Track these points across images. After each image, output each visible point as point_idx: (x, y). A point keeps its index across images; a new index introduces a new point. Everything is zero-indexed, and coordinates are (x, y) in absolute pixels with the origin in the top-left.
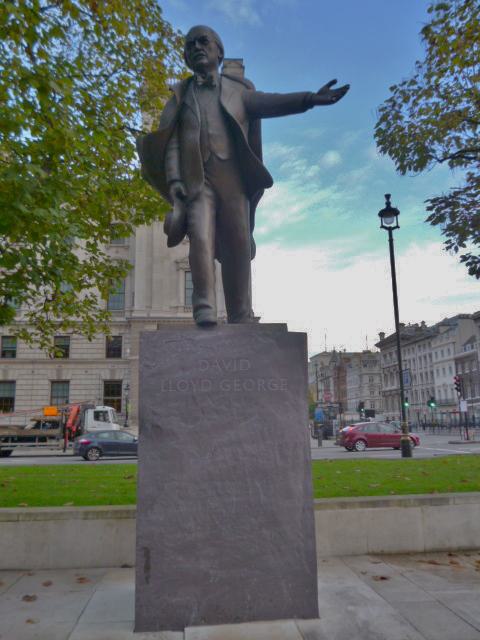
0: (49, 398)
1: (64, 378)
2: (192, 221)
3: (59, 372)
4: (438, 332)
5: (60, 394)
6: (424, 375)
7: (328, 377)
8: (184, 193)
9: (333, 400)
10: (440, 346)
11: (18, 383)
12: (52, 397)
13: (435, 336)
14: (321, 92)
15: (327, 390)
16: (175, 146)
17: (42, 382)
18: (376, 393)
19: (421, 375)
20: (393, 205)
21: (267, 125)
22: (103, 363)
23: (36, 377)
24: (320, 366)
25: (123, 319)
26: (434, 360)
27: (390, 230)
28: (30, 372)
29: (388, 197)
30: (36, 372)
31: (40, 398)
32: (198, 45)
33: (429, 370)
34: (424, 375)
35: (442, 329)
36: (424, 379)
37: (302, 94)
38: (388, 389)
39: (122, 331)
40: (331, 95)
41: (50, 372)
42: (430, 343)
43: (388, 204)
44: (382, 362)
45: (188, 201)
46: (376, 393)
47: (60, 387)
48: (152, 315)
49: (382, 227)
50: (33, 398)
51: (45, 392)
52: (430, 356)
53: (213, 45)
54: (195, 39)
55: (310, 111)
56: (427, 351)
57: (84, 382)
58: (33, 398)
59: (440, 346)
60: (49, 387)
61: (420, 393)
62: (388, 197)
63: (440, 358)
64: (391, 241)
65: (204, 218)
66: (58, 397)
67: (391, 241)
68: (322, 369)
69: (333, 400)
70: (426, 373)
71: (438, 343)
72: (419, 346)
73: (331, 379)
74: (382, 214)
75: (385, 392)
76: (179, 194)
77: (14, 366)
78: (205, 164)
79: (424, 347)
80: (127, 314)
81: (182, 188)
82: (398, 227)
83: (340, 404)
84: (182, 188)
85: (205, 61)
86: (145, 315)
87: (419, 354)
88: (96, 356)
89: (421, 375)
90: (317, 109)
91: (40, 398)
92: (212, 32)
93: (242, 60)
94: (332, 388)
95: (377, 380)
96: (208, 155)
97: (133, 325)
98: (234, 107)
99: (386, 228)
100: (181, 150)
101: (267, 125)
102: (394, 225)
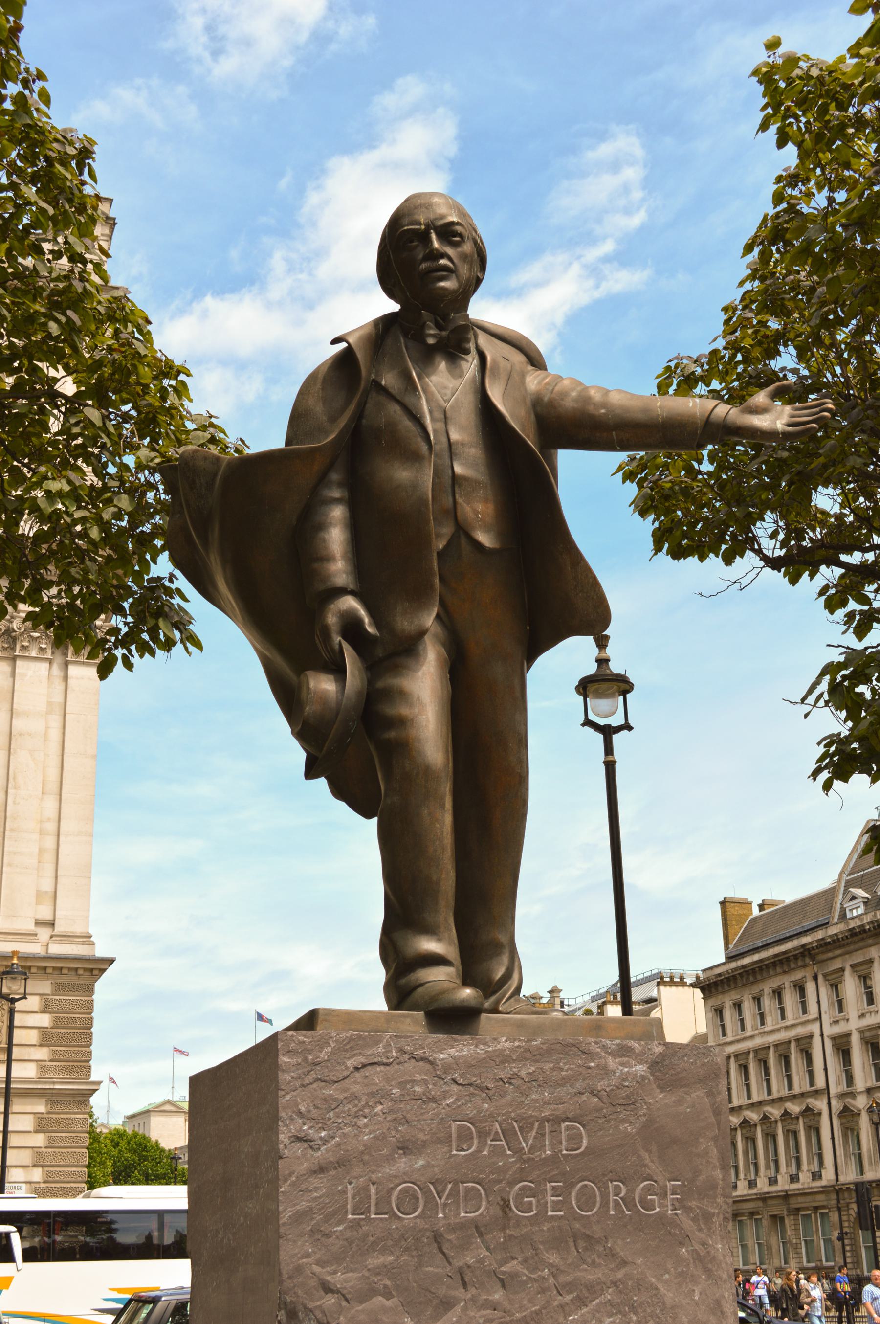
20: (615, 667)
27: (608, 732)
49: (588, 723)
64: (610, 767)
67: (610, 767)
82: (627, 727)
102: (617, 720)
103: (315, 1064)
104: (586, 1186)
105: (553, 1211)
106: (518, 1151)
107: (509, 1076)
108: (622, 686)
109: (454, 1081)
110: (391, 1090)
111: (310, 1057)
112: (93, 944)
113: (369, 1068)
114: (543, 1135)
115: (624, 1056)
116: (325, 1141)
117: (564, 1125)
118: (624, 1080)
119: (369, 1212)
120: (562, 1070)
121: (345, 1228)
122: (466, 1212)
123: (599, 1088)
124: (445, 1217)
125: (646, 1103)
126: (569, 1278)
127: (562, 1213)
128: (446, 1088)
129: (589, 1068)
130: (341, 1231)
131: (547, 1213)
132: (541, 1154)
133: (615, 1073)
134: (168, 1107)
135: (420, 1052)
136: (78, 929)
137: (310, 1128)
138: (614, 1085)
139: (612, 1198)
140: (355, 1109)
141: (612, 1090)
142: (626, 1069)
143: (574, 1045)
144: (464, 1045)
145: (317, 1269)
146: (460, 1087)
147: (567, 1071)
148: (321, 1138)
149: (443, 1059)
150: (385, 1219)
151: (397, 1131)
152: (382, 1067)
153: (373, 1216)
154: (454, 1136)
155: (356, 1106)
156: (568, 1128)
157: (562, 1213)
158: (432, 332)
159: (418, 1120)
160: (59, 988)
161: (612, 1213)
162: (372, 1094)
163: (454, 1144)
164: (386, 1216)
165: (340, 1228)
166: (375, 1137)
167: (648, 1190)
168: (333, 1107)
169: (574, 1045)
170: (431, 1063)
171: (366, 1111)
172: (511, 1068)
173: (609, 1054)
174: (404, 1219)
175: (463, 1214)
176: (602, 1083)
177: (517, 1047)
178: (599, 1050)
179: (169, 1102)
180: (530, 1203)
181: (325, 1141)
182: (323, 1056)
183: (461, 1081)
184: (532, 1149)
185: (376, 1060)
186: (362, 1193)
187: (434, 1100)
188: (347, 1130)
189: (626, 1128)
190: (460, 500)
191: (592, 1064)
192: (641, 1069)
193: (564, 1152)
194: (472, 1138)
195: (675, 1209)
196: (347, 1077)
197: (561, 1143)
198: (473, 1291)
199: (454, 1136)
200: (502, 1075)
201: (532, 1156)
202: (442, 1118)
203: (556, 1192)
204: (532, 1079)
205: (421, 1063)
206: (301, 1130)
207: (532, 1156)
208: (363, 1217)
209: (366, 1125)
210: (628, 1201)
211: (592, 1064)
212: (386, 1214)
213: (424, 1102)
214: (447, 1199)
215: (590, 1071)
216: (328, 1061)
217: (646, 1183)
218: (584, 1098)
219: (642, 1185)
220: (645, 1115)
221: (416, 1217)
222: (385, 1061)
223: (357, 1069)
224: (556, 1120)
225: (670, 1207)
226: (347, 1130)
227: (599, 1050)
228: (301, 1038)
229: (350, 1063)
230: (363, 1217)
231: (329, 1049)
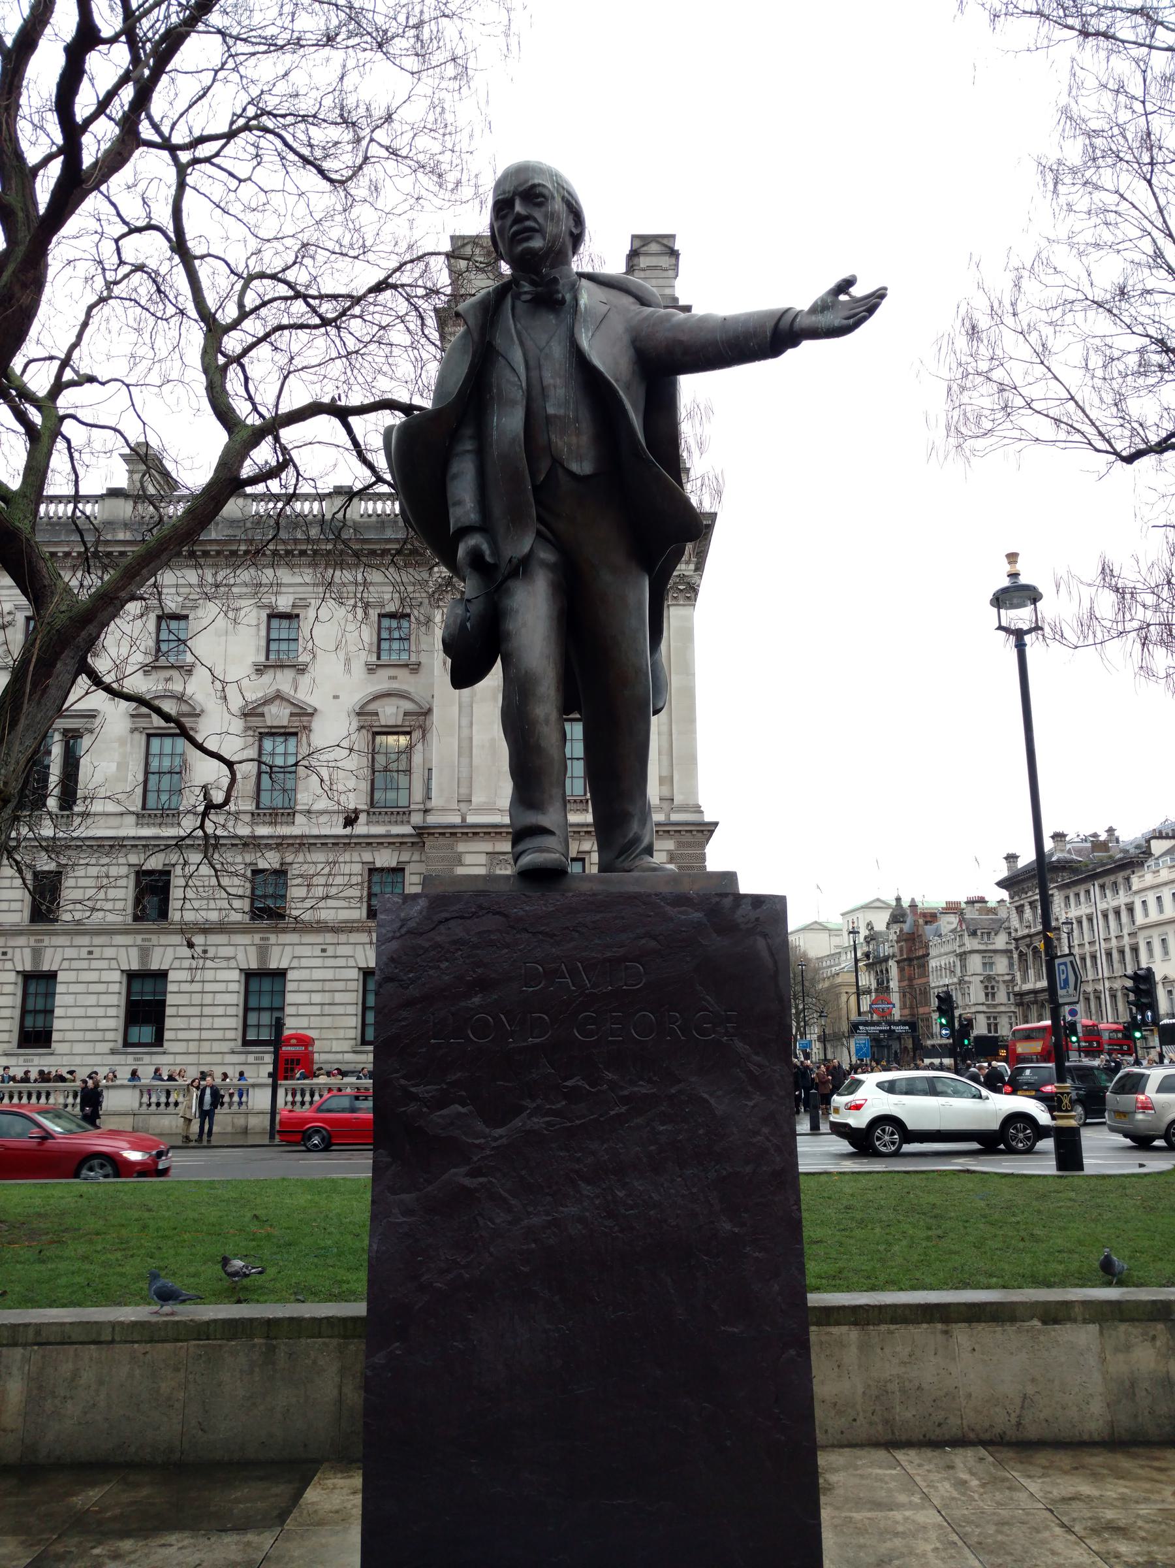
0: (17, 1013)
1: (154, 966)
2: (511, 626)
3: (263, 951)
4: (1148, 853)
5: (265, 1003)
6: (1115, 955)
7: (886, 959)
8: (489, 558)
9: (897, 1014)
10: (1152, 888)
11: (61, 977)
12: (247, 1010)
13: (1141, 864)
14: (820, 308)
15: (883, 988)
16: (469, 446)
17: (106, 976)
18: (1001, 996)
19: (1109, 954)
21: (692, 388)
22: (125, 932)
23: (95, 964)
24: (864, 932)
25: (407, 830)
26: (1140, 919)
27: (1019, 636)
28: (84, 953)
29: (1012, 557)
30: (97, 952)
31: (220, 1011)
32: (518, 208)
33: (1126, 940)
34: (1115, 955)
35: (1158, 847)
36: (1116, 965)
37: (769, 314)
38: (1027, 987)
39: (405, 857)
40: (844, 312)
41: (243, 952)
42: (1128, 879)
43: (1014, 575)
44: (1015, 922)
45: (495, 579)
46: (1001, 996)
47: (266, 985)
48: (471, 819)
49: (1000, 628)
50: (207, 1011)
51: (114, 999)
52: (1130, 909)
53: (558, 206)
54: (515, 194)
55: (790, 352)
56: (1122, 899)
57: (318, 974)
58: (207, 1011)
59: (1152, 888)
60: (238, 987)
61: (1106, 998)
62: (1012, 557)
63: (1154, 916)
65: (533, 613)
66: (260, 1009)
68: (869, 939)
69: (897, 1014)
70: (1122, 952)
71: (1149, 879)
72: (1102, 887)
73: (892, 964)
74: (1001, 600)
75: (1021, 995)
76: (476, 558)
77: (165, 939)
78: (535, 488)
79: (1078, 903)
80: (416, 819)
81: (485, 547)
83: (913, 1026)
84: (485, 547)
85: (537, 243)
86: (457, 820)
87: (1102, 906)
88: (344, 915)
89: (1109, 954)
90: (806, 344)
91: (220, 1011)
92: (555, 177)
93: (673, 236)
94: (894, 984)
95: (1001, 966)
96: (544, 466)
97: (429, 842)
98: (606, 352)
99: (1006, 630)
100: (481, 454)
101: (692, 388)
108: (1031, 595)
112: (702, 812)
126: (626, 1093)
134: (878, 904)
145: (403, 1082)
151: (474, 972)
158: (526, 289)
160: (680, 845)
162: (454, 942)
170: (506, 916)
179: (878, 900)
188: (431, 972)
190: (553, 437)
192: (697, 915)
198: (539, 1101)
226: (431, 972)
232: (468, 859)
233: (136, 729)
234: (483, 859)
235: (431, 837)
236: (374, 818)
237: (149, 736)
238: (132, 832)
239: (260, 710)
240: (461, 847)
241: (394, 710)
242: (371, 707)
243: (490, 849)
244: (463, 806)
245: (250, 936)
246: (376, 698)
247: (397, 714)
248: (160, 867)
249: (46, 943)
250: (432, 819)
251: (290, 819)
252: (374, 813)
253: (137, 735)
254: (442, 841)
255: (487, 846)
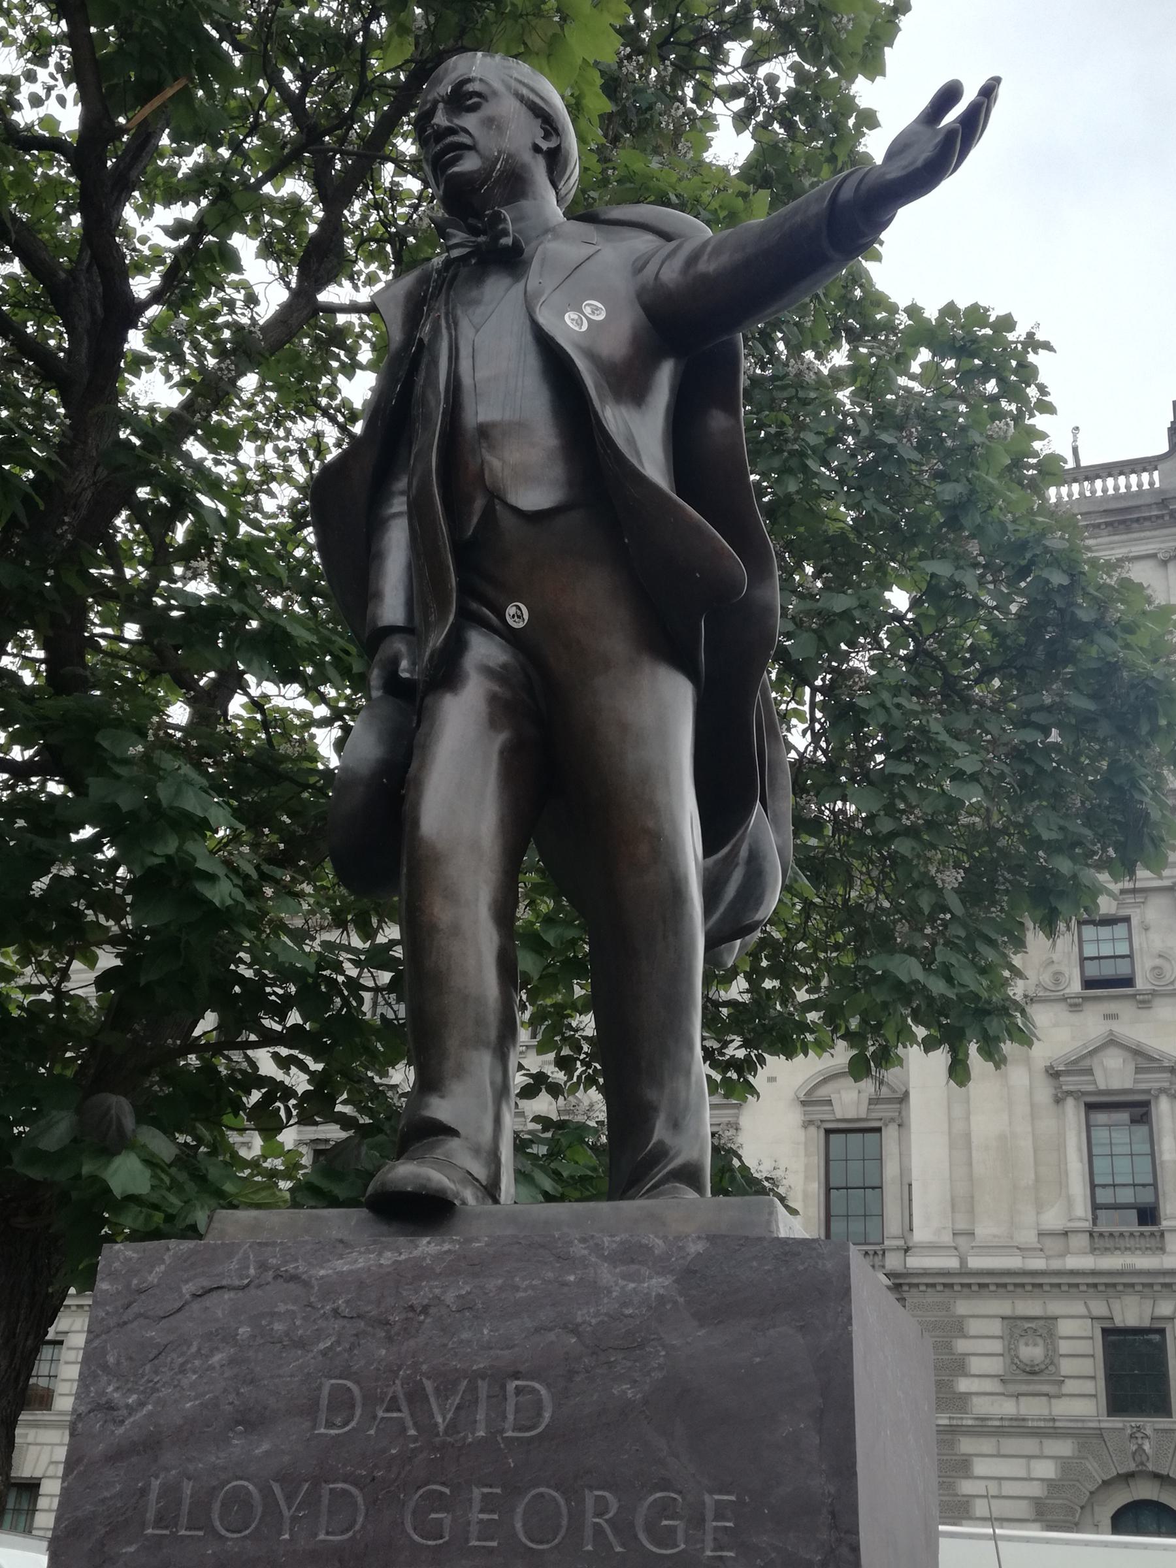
86: (952, 1263)
103: (140, 1292)
104: (542, 1495)
105: (188, 1528)
106: (427, 1428)
107: (426, 1301)
109: (336, 1313)
110: (237, 1329)
111: (135, 1282)
113: (215, 1294)
114: (476, 1401)
115: (633, 1261)
116: (131, 1410)
117: (512, 1385)
118: (625, 1305)
119: (176, 1525)
120: (517, 1288)
121: (137, 1551)
122: (328, 1533)
123: (579, 1320)
124: (291, 1540)
125: (664, 1347)
127: (495, 1544)
128: (322, 1323)
129: (565, 1284)
130: (132, 1553)
131: (467, 1540)
132: (465, 1438)
133: (610, 1292)
135: (291, 1267)
136: (1101, 1117)
137: (117, 1389)
138: (606, 1314)
139: (591, 1519)
140: (181, 1360)
141: (602, 1322)
142: (632, 1285)
143: (542, 1246)
144: (360, 1253)
146: (345, 1322)
147: (525, 1290)
148: (127, 1406)
149: (322, 1277)
150: (199, 1537)
152: (232, 1294)
153: (182, 1532)
154: (324, 1402)
155: (183, 1354)
156: (519, 1391)
157: (495, 1544)
159: (272, 1377)
161: (590, 1548)
163: (323, 1416)
164: (201, 1533)
165: (131, 1549)
166: (201, 1404)
167: (665, 1509)
168: (151, 1356)
169: (542, 1246)
171: (197, 1363)
172: (431, 1288)
173: (605, 1259)
174: (227, 1538)
175: (322, 1537)
176: (585, 1311)
177: (446, 1252)
178: (586, 1252)
180: (672, 1530)
181: (131, 1410)
182: (153, 1278)
183: (346, 1313)
184: (452, 1428)
185: (224, 1283)
186: (171, 1492)
187: (301, 1344)
189: (625, 1392)
191: (572, 1278)
192: (658, 1284)
193: (509, 1434)
194: (353, 1407)
195: (721, 1549)
196: (180, 1310)
197: (505, 1418)
199: (324, 1402)
200: (414, 1300)
201: (449, 1439)
202: (309, 1374)
203: (488, 1504)
204: (465, 1305)
205: (292, 1286)
206: (104, 1393)
207: (449, 1439)
208: (167, 1532)
209: (193, 1386)
210: (624, 1527)
211: (572, 1278)
212: (199, 1529)
213: (284, 1347)
214: (298, 1509)
215: (565, 1289)
216: (158, 1285)
217: (659, 1495)
218: (552, 1336)
219: (652, 1498)
220: (660, 1367)
221: (245, 1537)
222: (237, 1283)
223: (195, 1296)
224: (499, 1377)
225: (709, 1543)
226: (165, 1392)
227: (586, 1252)
228: (129, 1253)
229: (188, 1289)
230: (167, 1532)
231: (163, 1267)
232: (974, 1327)
233: (811, 1122)
234: (996, 1327)
235: (914, 1290)
236: (1100, 1243)
237: (828, 1132)
238: (1086, 1262)
239: (1085, 1064)
240: (962, 1307)
241: (854, 1095)
242: (823, 1092)
243: (1008, 1312)
244: (962, 1241)
245: (993, 1440)
246: (825, 1081)
247: (859, 1102)
248: (1146, 1323)
249: (30, 1439)
250: (915, 1262)
251: (1153, 1243)
252: (1101, 1235)
253: (812, 1130)
254: (931, 1297)
255: (1003, 1307)
